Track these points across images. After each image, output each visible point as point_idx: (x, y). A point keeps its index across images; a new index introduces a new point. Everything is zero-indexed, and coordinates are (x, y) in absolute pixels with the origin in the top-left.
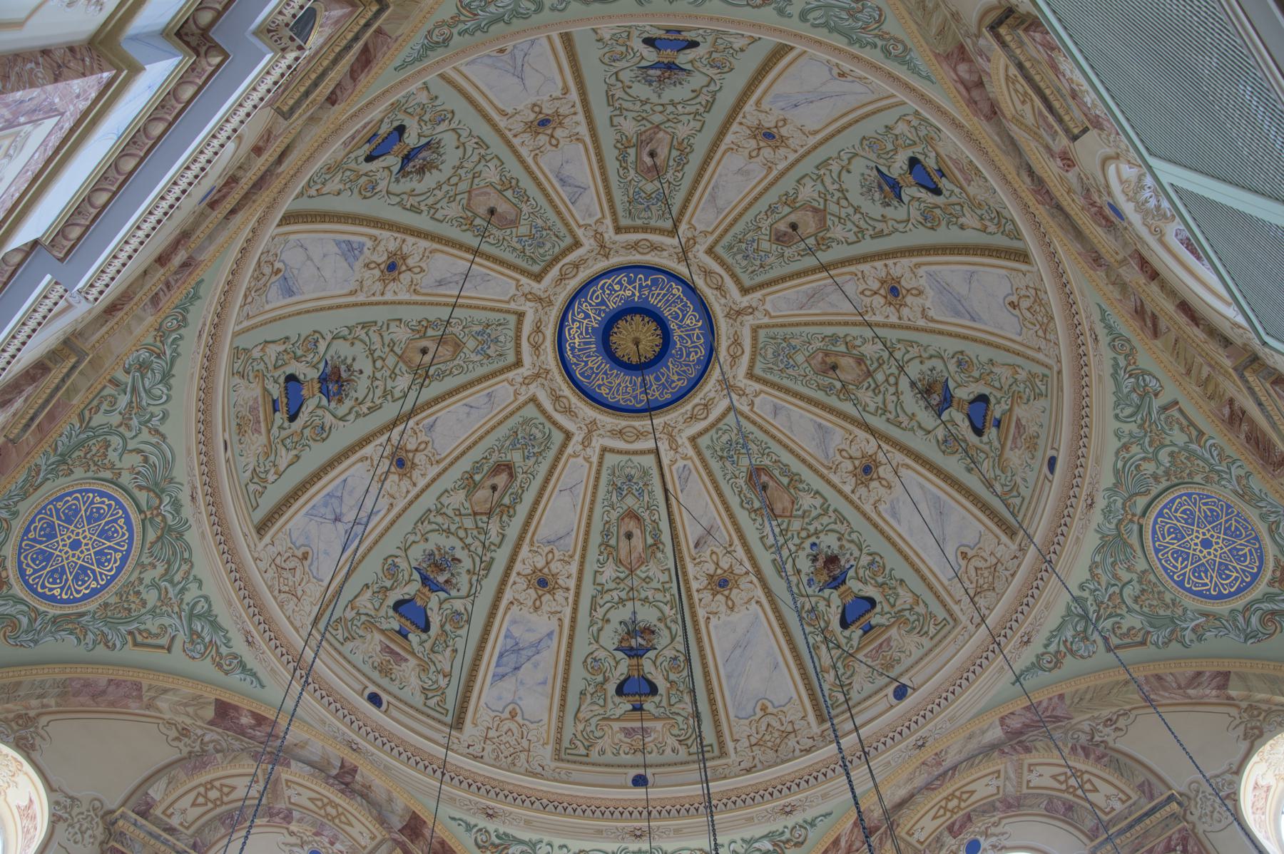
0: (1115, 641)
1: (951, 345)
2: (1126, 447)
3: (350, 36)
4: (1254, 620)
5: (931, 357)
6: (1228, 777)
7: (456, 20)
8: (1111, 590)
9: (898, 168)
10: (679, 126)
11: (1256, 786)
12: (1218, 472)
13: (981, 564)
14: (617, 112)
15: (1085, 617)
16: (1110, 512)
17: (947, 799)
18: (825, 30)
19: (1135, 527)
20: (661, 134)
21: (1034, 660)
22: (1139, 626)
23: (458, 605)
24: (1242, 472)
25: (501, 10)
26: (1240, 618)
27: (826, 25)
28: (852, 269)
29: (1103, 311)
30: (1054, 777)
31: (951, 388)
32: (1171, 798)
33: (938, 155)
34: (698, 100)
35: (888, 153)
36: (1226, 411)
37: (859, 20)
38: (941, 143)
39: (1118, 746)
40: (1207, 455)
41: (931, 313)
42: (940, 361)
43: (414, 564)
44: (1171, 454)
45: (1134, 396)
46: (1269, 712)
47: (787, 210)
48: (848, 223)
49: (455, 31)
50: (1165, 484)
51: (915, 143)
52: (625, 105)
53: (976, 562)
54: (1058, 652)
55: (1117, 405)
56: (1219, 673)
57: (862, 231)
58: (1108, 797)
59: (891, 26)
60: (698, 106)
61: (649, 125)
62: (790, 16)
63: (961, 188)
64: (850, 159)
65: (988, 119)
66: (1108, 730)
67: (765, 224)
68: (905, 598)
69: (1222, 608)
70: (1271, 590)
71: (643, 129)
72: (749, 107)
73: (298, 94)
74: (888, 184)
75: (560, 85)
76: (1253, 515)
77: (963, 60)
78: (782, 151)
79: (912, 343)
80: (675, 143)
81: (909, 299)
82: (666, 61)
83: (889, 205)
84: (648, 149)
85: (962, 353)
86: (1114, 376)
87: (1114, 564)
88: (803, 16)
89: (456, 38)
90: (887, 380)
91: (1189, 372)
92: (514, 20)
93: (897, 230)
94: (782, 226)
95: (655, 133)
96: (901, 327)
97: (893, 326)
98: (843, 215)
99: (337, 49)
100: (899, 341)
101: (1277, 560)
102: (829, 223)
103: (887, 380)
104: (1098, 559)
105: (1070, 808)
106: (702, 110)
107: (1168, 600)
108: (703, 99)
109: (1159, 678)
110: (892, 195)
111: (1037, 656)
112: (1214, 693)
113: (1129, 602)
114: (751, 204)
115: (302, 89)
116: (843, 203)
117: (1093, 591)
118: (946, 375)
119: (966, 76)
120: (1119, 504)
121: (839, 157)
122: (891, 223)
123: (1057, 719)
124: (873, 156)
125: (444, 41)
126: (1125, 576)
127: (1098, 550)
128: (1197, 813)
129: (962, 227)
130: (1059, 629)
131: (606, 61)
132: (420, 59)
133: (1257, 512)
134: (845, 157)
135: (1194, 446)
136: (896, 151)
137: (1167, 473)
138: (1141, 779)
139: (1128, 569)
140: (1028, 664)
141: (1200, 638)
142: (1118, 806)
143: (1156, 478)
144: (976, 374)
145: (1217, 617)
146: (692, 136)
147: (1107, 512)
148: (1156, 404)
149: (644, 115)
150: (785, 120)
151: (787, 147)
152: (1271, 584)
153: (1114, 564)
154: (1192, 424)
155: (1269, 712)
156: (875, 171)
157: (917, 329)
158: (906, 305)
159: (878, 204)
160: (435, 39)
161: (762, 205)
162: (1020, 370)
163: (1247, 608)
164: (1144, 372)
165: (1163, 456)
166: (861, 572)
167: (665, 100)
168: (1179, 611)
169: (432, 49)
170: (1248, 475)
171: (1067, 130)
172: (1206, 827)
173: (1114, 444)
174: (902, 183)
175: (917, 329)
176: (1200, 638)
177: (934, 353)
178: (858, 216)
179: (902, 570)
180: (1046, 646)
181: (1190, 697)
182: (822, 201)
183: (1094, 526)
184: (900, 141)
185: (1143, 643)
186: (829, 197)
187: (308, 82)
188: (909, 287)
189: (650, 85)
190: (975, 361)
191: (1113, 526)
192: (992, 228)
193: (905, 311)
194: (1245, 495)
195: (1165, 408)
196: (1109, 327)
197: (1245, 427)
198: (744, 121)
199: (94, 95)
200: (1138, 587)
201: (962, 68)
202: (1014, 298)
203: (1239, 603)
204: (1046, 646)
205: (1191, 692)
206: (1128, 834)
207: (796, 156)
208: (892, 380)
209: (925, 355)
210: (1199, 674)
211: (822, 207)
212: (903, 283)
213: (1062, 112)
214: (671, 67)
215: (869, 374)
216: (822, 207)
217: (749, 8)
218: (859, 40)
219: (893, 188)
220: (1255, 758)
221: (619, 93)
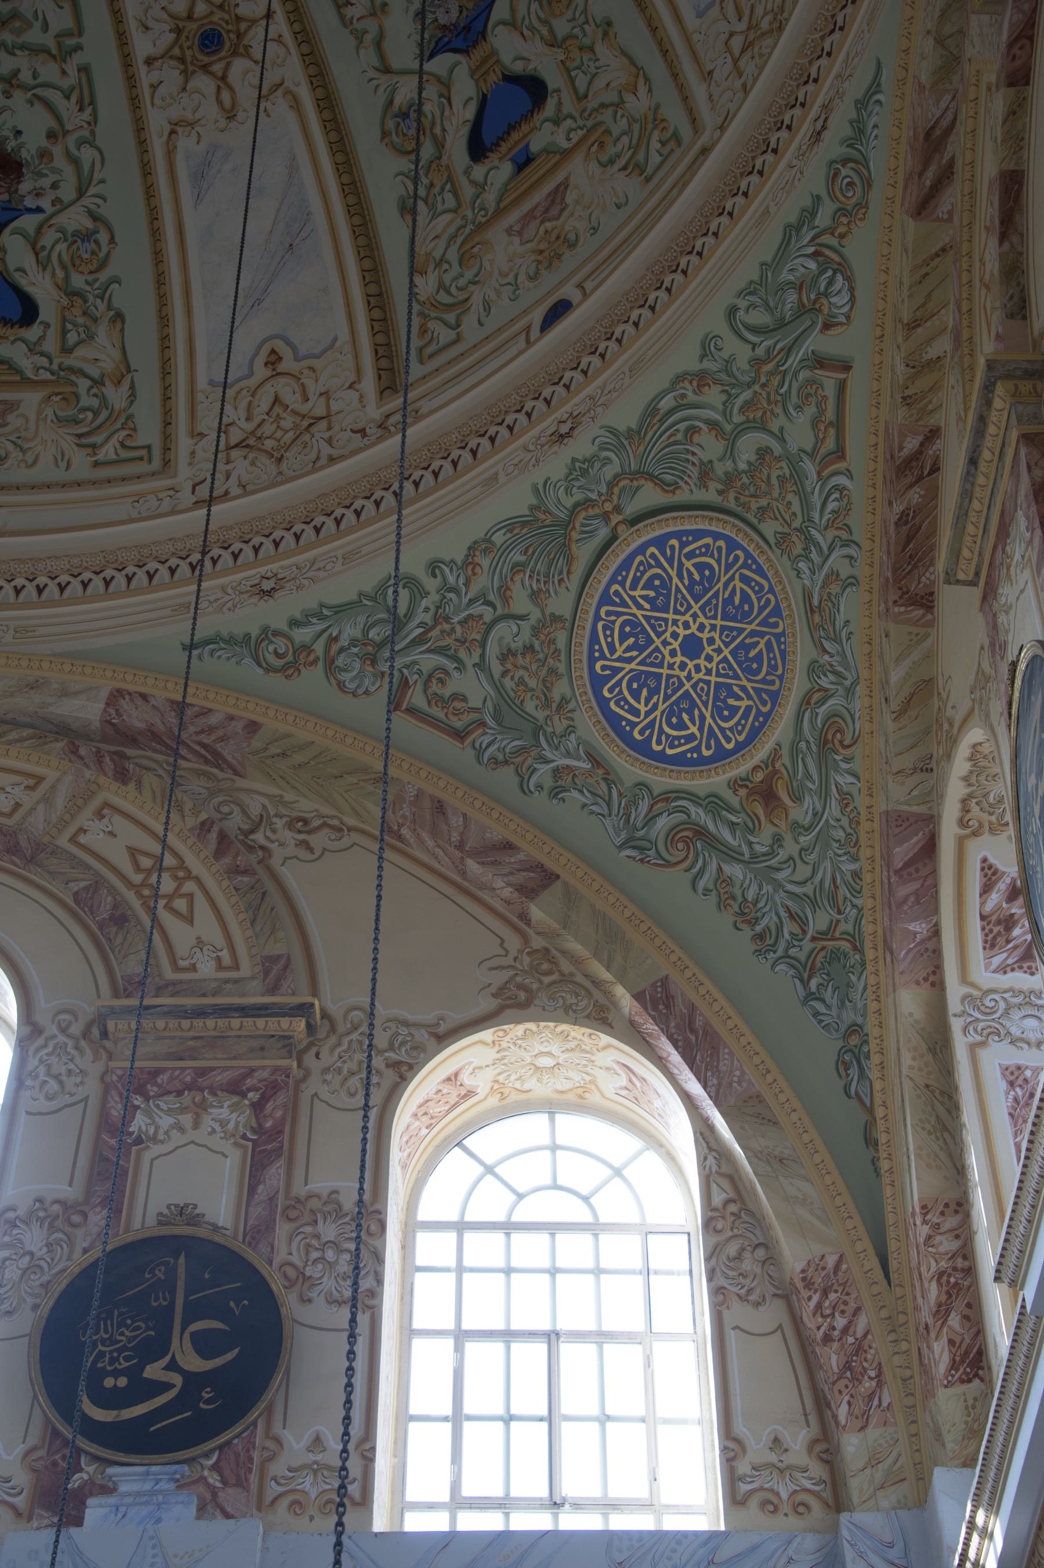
0: (417, 698)
2: (702, 380)
4: (663, 823)
6: (421, 1036)
8: (478, 609)
11: (453, 1079)
12: (809, 540)
13: (292, 399)
15: (397, 623)
16: (584, 473)
19: (603, 533)
21: (255, 633)
22: (475, 702)
23: (75, 219)
24: (845, 571)
26: (644, 806)
29: (875, 87)
30: (133, 852)
32: (303, 1010)
36: (912, 444)
39: (286, 873)
40: (816, 500)
44: (763, 453)
45: (792, 297)
46: (566, 979)
50: (710, 496)
53: (285, 388)
54: (307, 648)
55: (750, 290)
56: (540, 867)
58: (200, 943)
59: (312, 680)
66: (288, 836)
68: (100, 353)
69: (630, 769)
70: (728, 795)
76: (802, 651)
86: (792, 231)
87: (518, 568)
91: (913, 326)
101: (775, 754)
104: (499, 538)
105: (120, 919)
107: (556, 695)
109: (440, 808)
111: (265, 630)
112: (507, 892)
113: (493, 650)
117: (446, 588)
120: (610, 471)
123: (217, 759)
126: (521, 602)
127: (511, 525)
128: (327, 1059)
130: (340, 610)
133: (813, 653)
135: (809, 467)
137: (729, 479)
138: (279, 949)
139: (535, 596)
140: (239, 630)
141: (555, 793)
142: (206, 968)
143: (705, 473)
145: (610, 778)
147: (580, 469)
148: (816, 342)
152: (734, 785)
153: (518, 568)
154: (839, 425)
155: (566, 979)
163: (667, 796)
164: (843, 268)
165: (748, 446)
166: (49, 238)
168: (560, 726)
170: (853, 581)
172: (324, 1091)
173: (686, 358)
176: (555, 793)
179: (134, 296)
180: (294, 623)
181: (463, 874)
183: (538, 476)
185: (460, 735)
191: (569, 502)
194: (818, 612)
195: (820, 362)
196: (859, 128)
197: (915, 496)
200: (526, 636)
203: (662, 780)
204: (294, 623)
205: (472, 866)
206: (186, 1023)
210: (508, 847)
220: (487, 1035)
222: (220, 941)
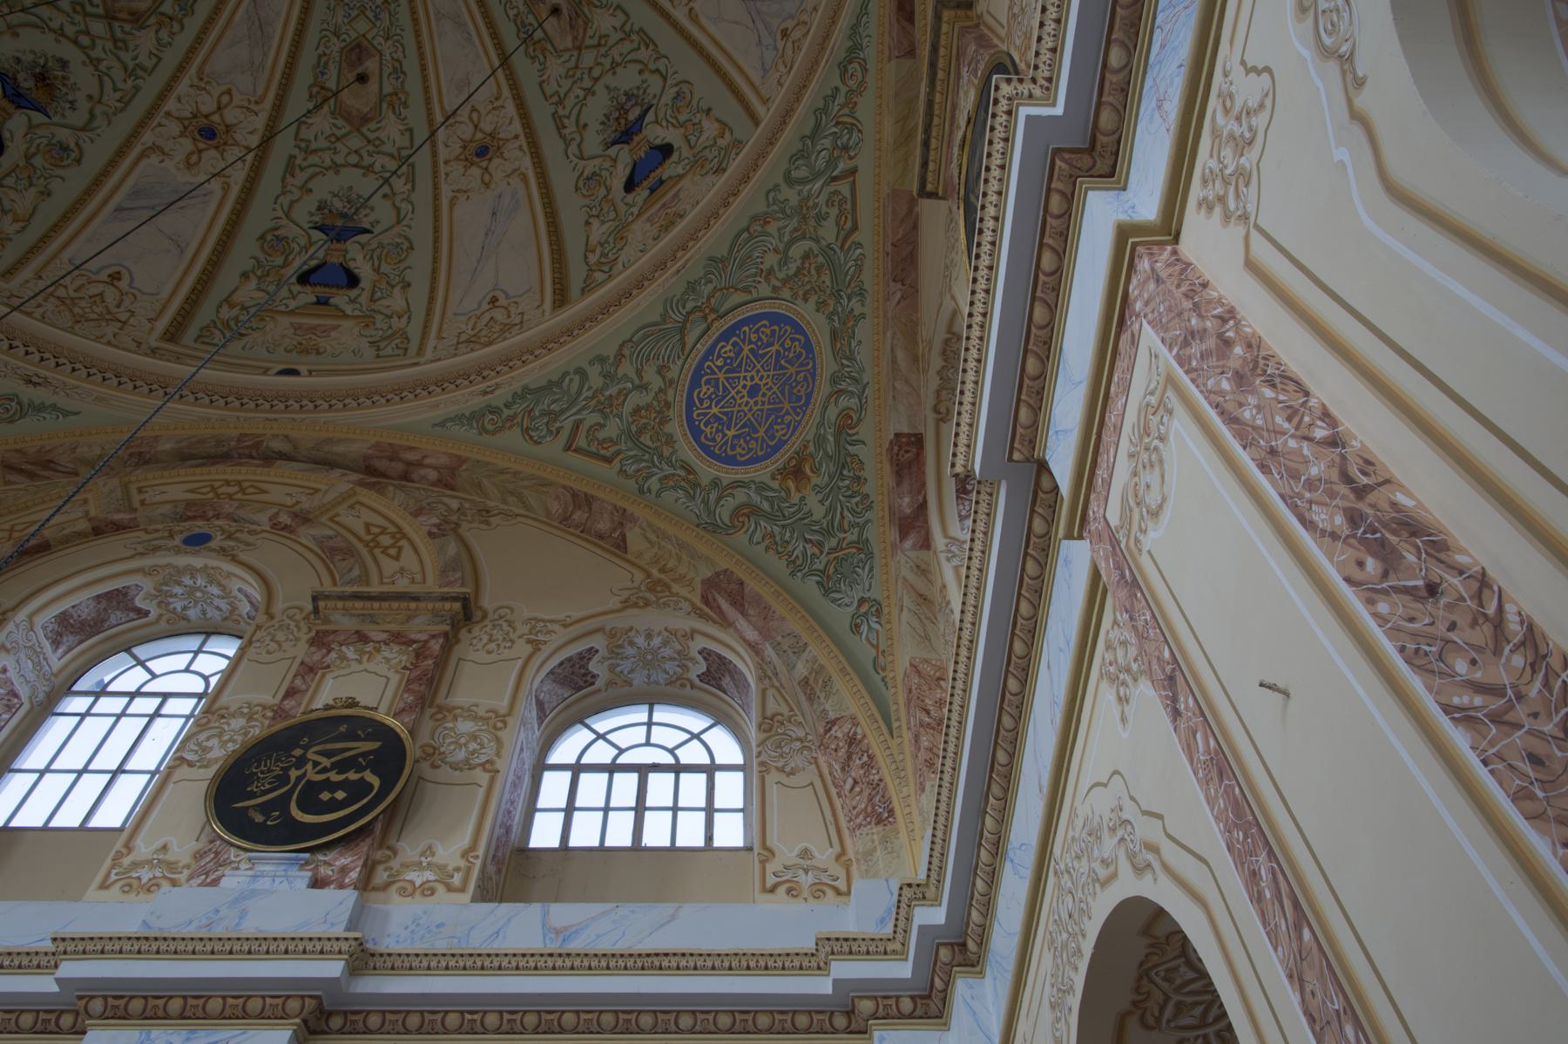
1: (97, 152)
3: (934, 143)
5: (92, 116)
7: (851, 104)
9: (356, 256)
10: (563, 71)
14: (627, 28)
17: (228, 483)
18: (555, 378)
20: (569, 44)
25: (819, 148)
27: (559, 383)
28: (268, 104)
29: (66, 414)
30: (367, 526)
31: (33, 114)
33: (346, 316)
34: (573, 118)
35: (379, 259)
37: (542, 415)
38: (356, 331)
41: (154, 159)
42: (80, 124)
43: (306, 226)
47: (387, 89)
48: (325, 144)
49: (844, 89)
51: (372, 300)
52: (627, 46)
57: (308, 152)
59: (513, 438)
60: (566, 112)
61: (588, 42)
62: (591, 363)
63: (292, 312)
64: (398, 210)
65: (366, 458)
67: (387, 48)
71: (590, 32)
72: (527, 163)
73: (943, 42)
74: (345, 229)
75: (704, 21)
77: (440, 481)
78: (456, 149)
79: (126, 102)
80: (549, 47)
81: (187, 145)
82: (637, 139)
83: (319, 208)
84: (565, 11)
85: (78, 161)
88: (581, 372)
89: (837, 82)
90: (87, 33)
92: (800, 146)
93: (284, 193)
94: (371, 65)
95: (575, 38)
96: (155, 107)
97: (162, 97)
98: (339, 145)
99: (936, 121)
100: (137, 89)
102: (340, 122)
103: (87, 33)
106: (561, 112)
108: (570, 125)
110: (328, 222)
114: (422, 57)
115: (942, 51)
116: (353, 159)
118: (56, 119)
119: (422, 472)
121: (407, 200)
122: (297, 194)
124: (385, 239)
125: (846, 71)
129: (245, 276)
131: (685, 87)
132: (854, 29)
134: (405, 207)
136: (377, 270)
144: (38, 161)
146: (542, 71)
149: (603, 50)
150: (487, 185)
151: (457, 159)
156: (368, 226)
157: (142, 125)
158: (182, 135)
159: (329, 197)
160: (855, 65)
161: (411, 65)
162: (18, 226)
167: (599, 87)
169: (851, 50)
171: (327, 597)
174: (336, 245)
175: (142, 125)
177: (95, 124)
178: (328, 162)
182: (372, 136)
184: (384, 285)
186: (371, 148)
187: (941, 63)
188: (205, 155)
189: (626, 94)
190: (58, 172)
192: (226, 313)
193: (174, 128)
196: (41, 408)
198: (517, 143)
199: (1112, 389)
201: (433, 475)
202: (123, 284)
207: (441, 160)
208: (85, 40)
209: (99, 109)
211: (364, 130)
212: (213, 153)
213: (349, 604)
214: (626, 136)
215: (110, 17)
216: (364, 130)
217: (627, 336)
218: (522, 397)
219: (340, 228)
221: (643, 54)
222: (416, 568)
